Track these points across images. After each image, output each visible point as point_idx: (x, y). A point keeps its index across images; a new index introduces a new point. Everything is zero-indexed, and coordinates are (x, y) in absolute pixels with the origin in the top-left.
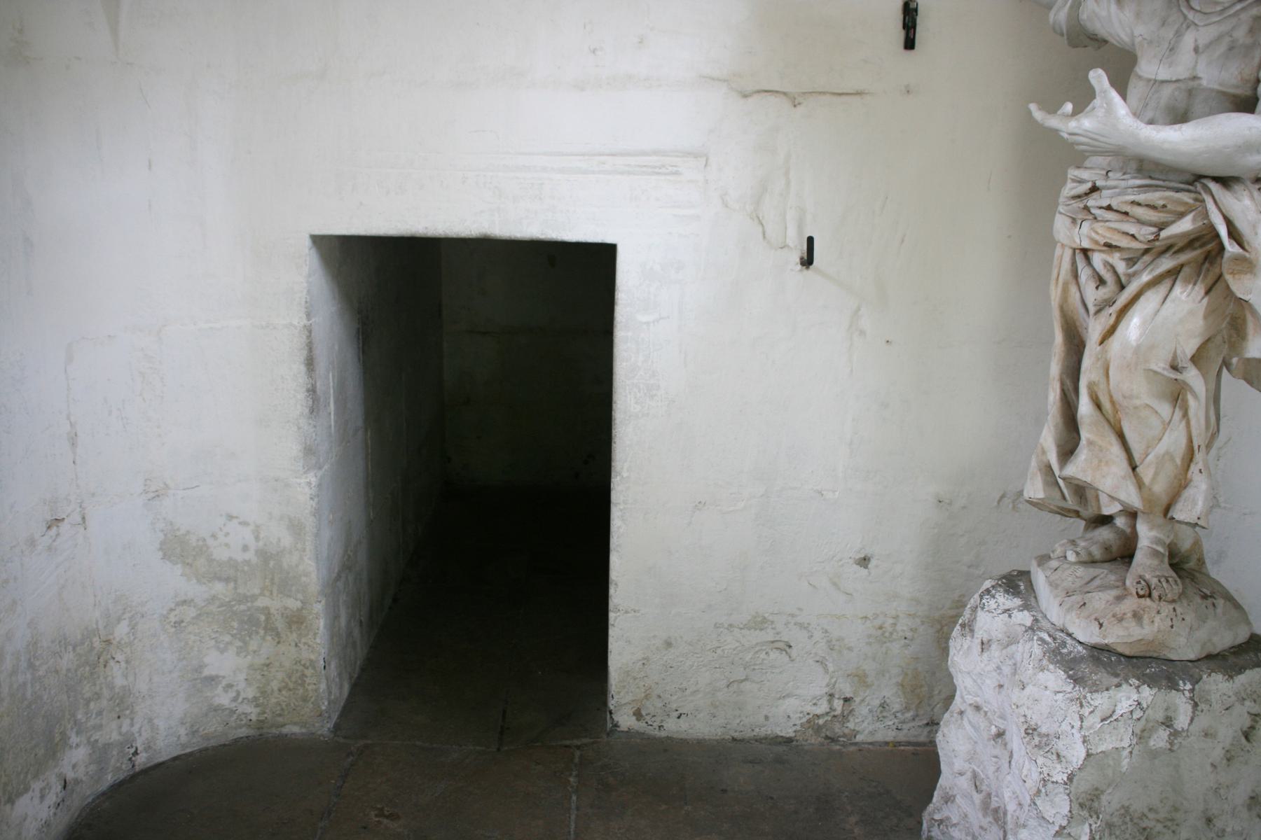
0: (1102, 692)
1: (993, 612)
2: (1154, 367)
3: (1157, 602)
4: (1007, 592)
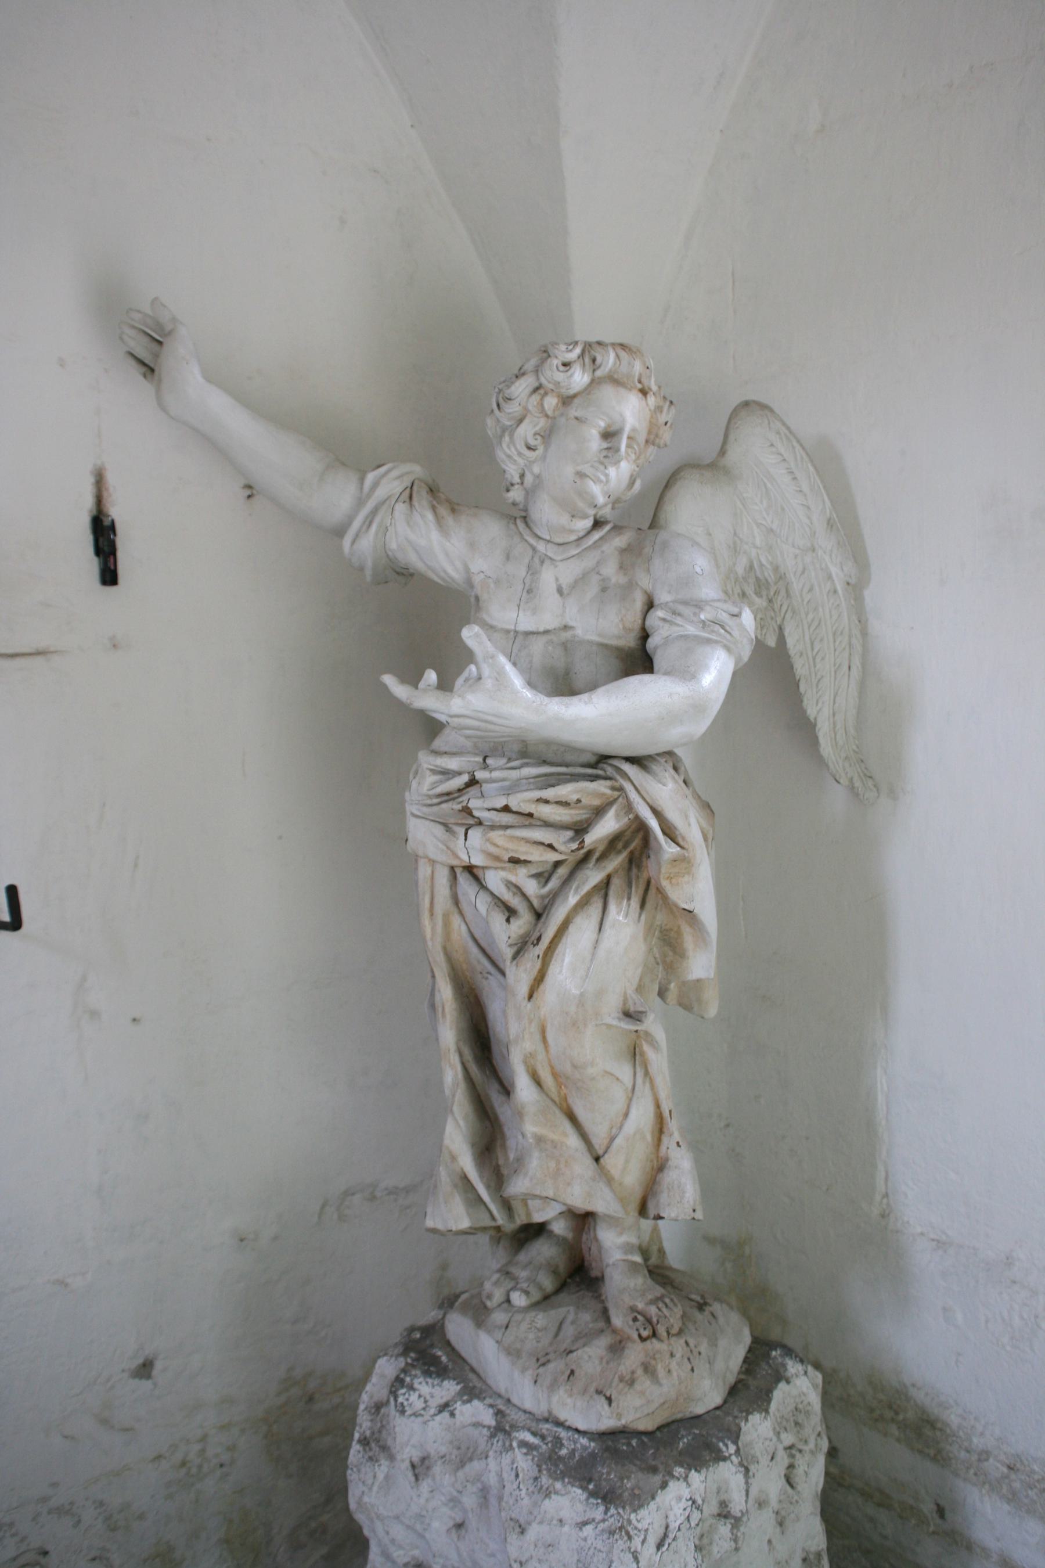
0: (648, 1504)
1: (422, 1415)
3: (666, 1342)
4: (427, 1373)
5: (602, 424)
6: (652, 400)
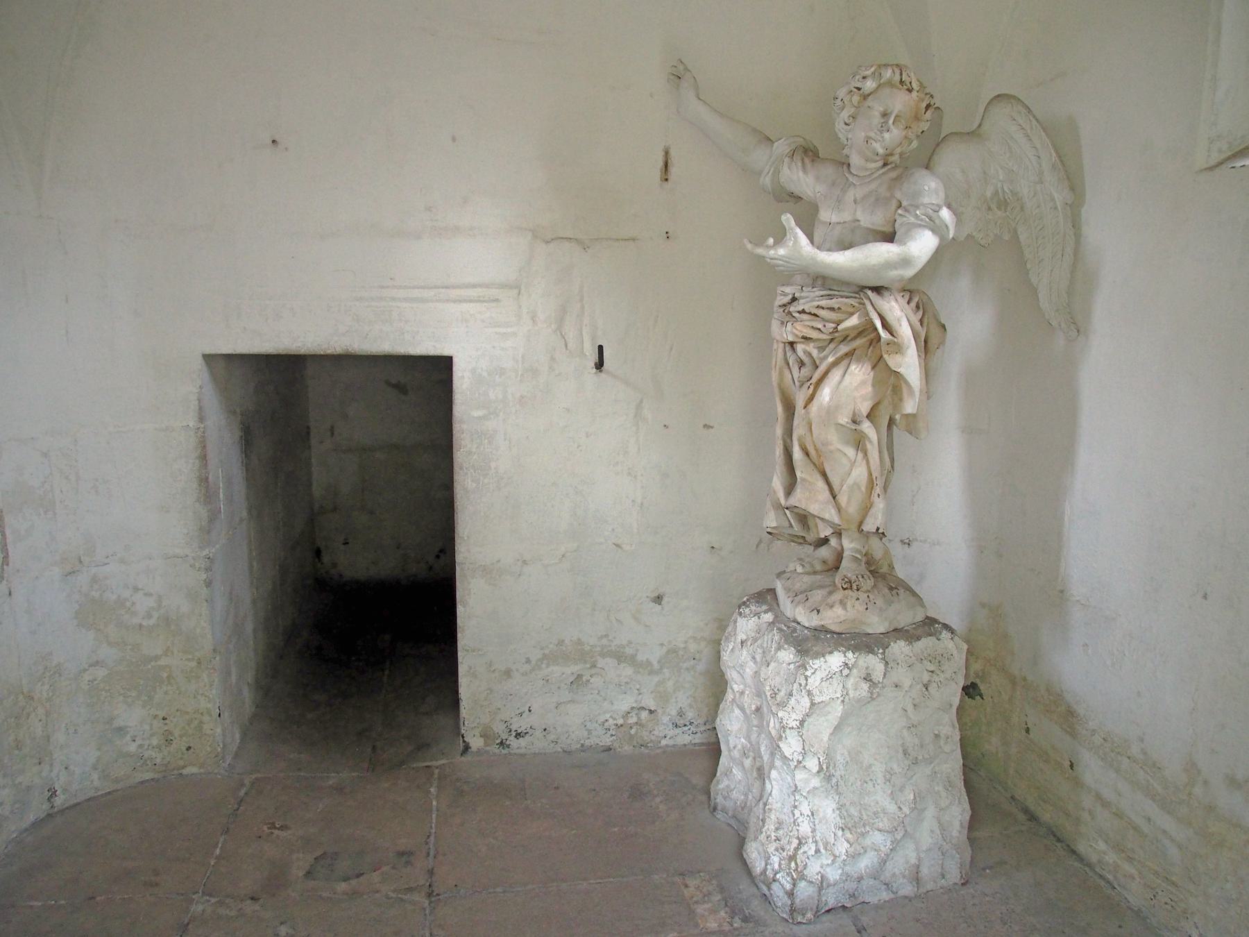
2: (841, 422)
5: (882, 109)
6: (914, 94)
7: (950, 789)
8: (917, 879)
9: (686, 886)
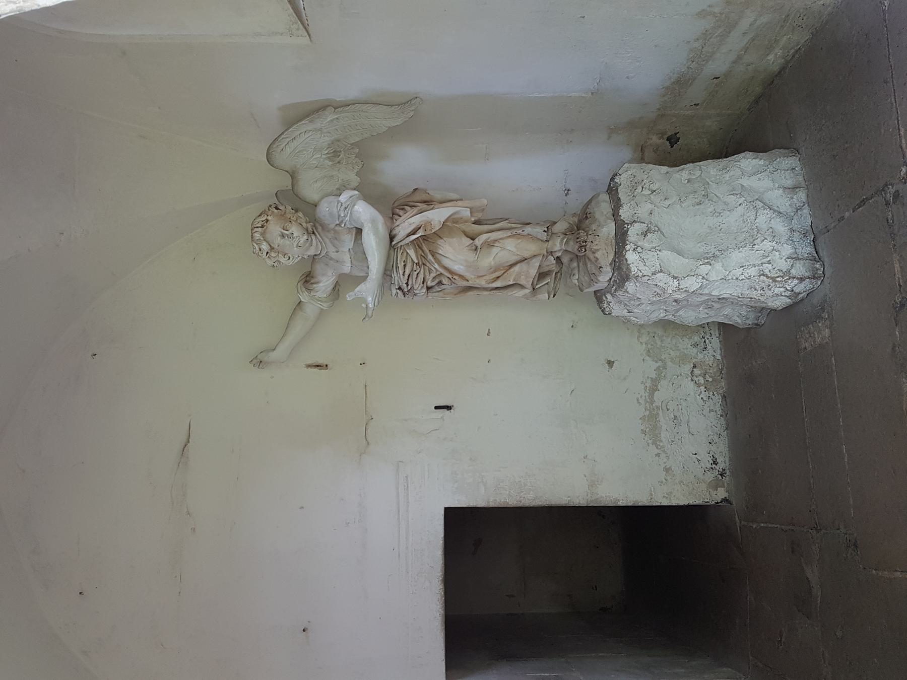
5: (279, 238)
6: (269, 218)
7: (728, 169)
8: (794, 189)
9: (805, 348)
